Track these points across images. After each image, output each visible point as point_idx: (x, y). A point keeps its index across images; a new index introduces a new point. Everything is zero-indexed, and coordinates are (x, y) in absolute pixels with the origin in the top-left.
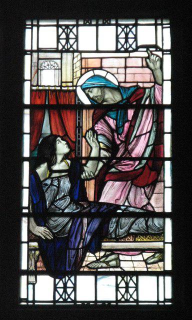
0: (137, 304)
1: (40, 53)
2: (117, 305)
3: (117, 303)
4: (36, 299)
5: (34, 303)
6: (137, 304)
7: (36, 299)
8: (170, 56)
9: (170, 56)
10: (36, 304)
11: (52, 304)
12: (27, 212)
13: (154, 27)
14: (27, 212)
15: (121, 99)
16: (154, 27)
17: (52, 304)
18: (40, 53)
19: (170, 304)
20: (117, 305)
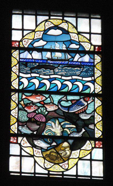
0: (35, 175)
1: (38, 17)
2: (91, 179)
3: (63, 177)
4: (23, 171)
5: (63, 177)
6: (35, 175)
7: (23, 171)
8: (11, 170)
9: (11, 170)
10: (23, 175)
11: (47, 176)
12: (51, 17)
13: (19, 154)
14: (51, 17)
15: (77, 61)
16: (19, 154)
17: (47, 176)
18: (38, 17)
19: (102, 179)
20: (91, 179)
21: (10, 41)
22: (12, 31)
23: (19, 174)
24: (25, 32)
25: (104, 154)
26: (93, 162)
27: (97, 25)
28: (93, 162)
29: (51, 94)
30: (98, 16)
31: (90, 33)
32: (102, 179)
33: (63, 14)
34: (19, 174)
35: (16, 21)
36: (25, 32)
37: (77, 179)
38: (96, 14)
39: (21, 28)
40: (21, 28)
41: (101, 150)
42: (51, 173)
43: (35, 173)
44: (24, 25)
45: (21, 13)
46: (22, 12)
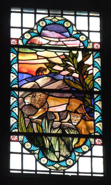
0: (64, 174)
5: (50, 173)
6: (50, 173)
7: (24, 169)
9: (11, 168)
13: (20, 152)
21: (8, 38)
22: (11, 29)
23: (34, 173)
24: (24, 30)
25: (105, 150)
26: (93, 158)
27: (95, 22)
28: (93, 158)
29: (81, 90)
30: (85, 13)
31: (89, 31)
32: (102, 175)
33: (35, 11)
34: (34, 173)
35: (15, 18)
36: (24, 30)
37: (78, 176)
38: (95, 11)
39: (87, 29)
40: (20, 26)
41: (101, 147)
42: (52, 170)
43: (36, 171)
44: (21, 22)
45: (34, 12)
46: (74, 12)
